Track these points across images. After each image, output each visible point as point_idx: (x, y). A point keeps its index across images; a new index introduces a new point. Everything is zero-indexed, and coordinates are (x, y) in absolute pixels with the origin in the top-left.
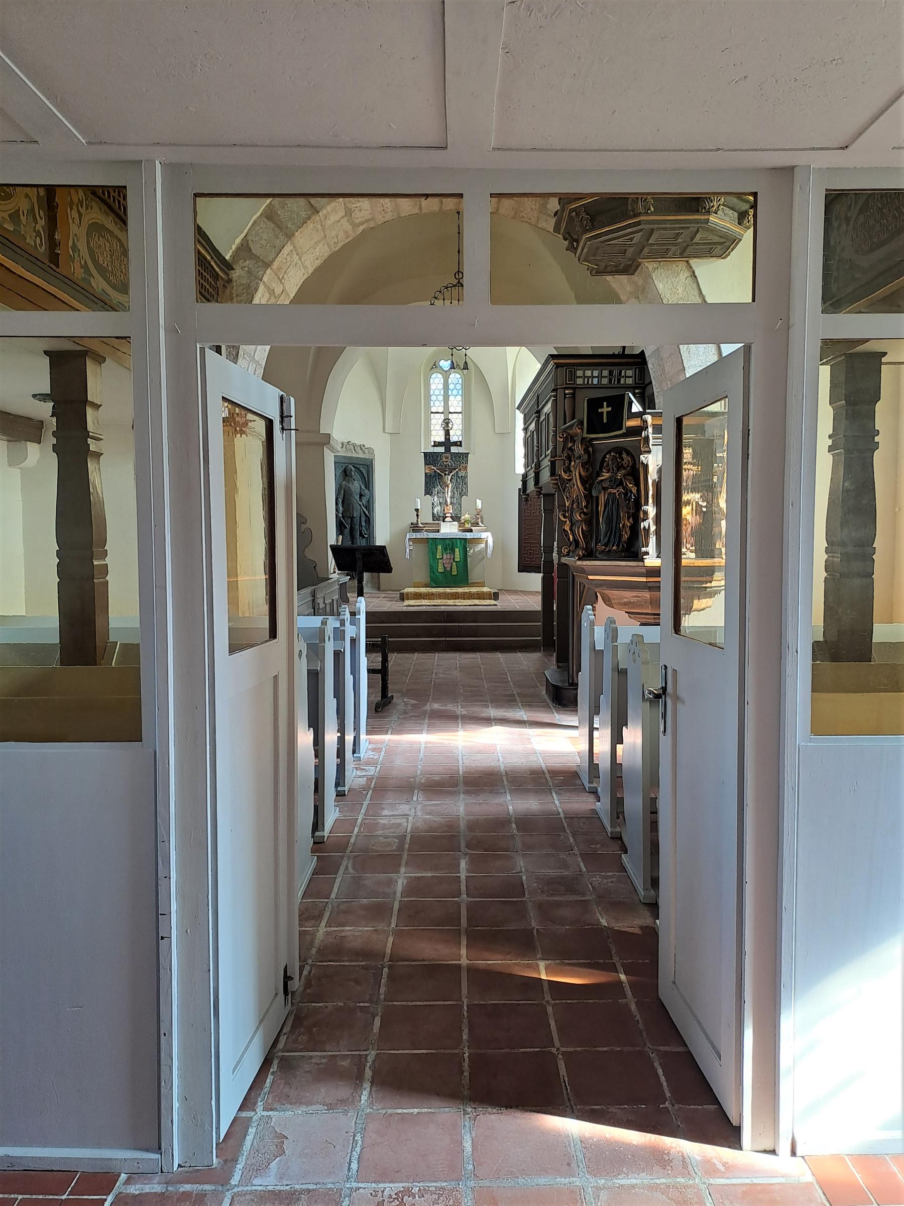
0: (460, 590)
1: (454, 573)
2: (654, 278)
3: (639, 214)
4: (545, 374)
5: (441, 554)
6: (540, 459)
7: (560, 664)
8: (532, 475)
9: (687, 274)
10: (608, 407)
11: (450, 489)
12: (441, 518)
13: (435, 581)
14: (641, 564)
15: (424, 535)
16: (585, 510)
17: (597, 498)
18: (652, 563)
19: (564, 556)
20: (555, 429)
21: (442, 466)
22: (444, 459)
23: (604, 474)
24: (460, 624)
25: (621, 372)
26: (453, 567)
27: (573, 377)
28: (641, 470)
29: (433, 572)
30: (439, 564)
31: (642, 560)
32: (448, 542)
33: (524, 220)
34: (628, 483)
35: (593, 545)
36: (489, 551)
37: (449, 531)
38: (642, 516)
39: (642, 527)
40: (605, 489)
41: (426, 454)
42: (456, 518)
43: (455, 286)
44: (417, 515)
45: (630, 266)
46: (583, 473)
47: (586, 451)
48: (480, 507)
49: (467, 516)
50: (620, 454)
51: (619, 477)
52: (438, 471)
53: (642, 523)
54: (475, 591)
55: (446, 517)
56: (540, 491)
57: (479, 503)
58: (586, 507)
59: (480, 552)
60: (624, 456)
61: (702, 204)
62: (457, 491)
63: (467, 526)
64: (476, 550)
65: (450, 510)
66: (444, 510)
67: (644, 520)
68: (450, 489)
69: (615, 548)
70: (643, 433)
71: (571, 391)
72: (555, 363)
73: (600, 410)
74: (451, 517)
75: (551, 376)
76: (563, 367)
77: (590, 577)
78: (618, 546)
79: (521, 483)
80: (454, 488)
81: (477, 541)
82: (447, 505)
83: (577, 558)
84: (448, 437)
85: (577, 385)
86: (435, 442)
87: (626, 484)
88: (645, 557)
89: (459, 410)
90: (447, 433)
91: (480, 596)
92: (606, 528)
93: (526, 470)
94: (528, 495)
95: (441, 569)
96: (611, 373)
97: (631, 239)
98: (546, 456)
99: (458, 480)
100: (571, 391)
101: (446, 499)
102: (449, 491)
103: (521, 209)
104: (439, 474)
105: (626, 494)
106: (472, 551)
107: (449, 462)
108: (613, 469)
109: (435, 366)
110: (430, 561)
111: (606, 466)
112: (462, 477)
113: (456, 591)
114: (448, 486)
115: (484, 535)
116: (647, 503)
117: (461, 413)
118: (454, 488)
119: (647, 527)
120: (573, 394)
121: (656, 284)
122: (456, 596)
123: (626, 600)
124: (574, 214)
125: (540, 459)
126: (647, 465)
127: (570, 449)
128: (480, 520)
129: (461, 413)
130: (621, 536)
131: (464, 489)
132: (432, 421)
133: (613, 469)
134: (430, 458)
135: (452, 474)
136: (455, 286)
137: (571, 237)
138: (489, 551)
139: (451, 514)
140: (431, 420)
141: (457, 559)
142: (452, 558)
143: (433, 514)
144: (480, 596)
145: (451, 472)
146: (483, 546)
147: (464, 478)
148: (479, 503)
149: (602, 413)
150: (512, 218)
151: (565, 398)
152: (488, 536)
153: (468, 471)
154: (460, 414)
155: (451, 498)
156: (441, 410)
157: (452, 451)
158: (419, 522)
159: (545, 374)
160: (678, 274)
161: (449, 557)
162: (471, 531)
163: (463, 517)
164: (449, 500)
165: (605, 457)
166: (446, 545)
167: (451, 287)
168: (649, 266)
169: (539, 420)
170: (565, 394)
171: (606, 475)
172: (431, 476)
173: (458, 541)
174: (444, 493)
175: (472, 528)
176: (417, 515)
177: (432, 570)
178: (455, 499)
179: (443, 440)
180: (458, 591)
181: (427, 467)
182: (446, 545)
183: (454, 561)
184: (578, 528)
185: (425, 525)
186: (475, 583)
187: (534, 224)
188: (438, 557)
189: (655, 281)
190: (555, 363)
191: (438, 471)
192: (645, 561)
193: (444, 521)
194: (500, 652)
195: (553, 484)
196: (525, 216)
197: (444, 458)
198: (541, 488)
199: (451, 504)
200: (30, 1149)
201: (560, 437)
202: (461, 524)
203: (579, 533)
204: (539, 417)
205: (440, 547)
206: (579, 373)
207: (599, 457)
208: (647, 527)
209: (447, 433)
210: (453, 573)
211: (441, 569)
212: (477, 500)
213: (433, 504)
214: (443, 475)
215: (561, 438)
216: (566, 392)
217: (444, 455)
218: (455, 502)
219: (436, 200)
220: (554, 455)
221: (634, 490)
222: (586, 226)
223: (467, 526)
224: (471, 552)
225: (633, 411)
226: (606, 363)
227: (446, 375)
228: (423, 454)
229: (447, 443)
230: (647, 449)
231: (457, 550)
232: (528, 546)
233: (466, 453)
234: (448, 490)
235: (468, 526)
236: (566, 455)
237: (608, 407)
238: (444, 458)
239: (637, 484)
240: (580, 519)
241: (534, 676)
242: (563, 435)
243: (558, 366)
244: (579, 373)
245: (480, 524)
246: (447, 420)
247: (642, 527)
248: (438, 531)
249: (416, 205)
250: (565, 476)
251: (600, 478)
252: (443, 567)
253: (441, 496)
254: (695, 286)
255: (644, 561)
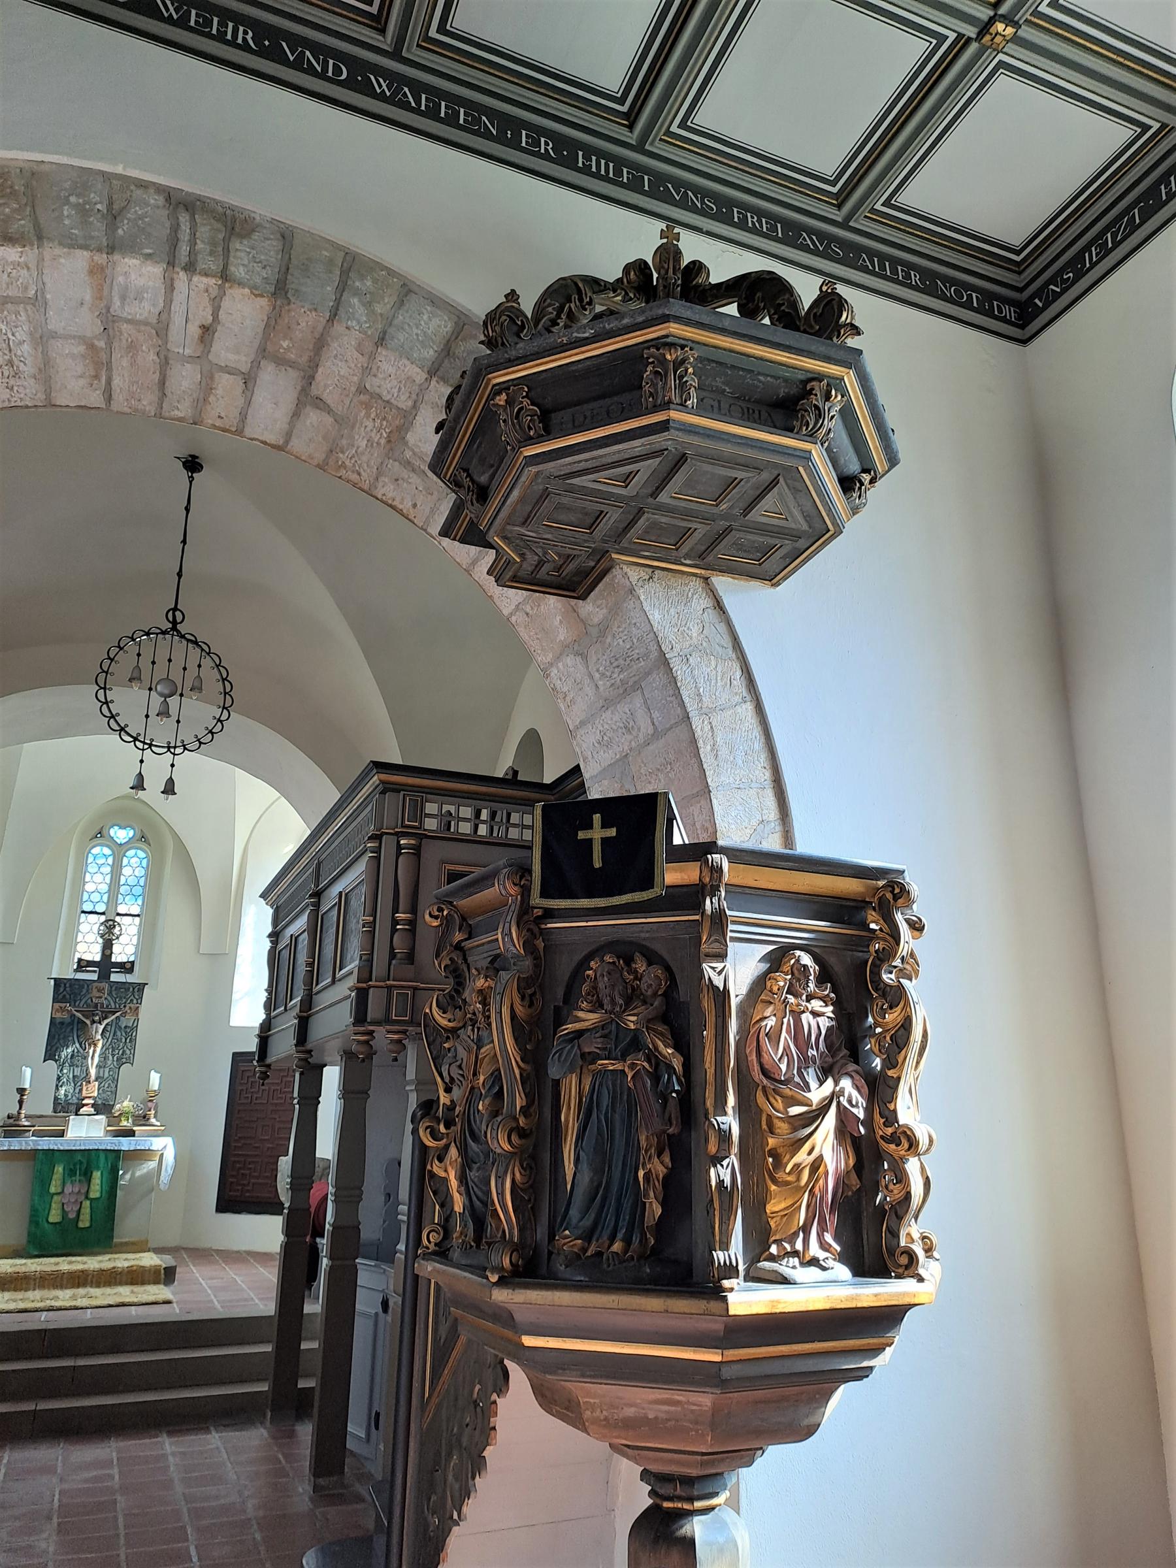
0: (92, 1263)
1: (85, 1223)
2: (642, 598)
3: (666, 405)
4: (295, 871)
5: (59, 1183)
6: (273, 1014)
7: (321, 1481)
8: (288, 1023)
9: (706, 602)
10: (604, 826)
11: (98, 1050)
12: (73, 1108)
13: (38, 1246)
14: (714, 1306)
15: (29, 1142)
16: (522, 1121)
17: (557, 1083)
18: (750, 1304)
19: (427, 1256)
20: (371, 918)
21: (88, 1006)
22: (95, 993)
23: (581, 1014)
24: (81, 1362)
25: (509, 815)
26: (83, 1211)
27: (419, 814)
28: (707, 1003)
29: (37, 1224)
30: (53, 1205)
31: (718, 1294)
32: (79, 1157)
33: (342, 472)
34: (660, 1044)
35: (542, 1232)
36: (165, 1177)
37: (84, 1135)
38: (712, 1148)
39: (713, 1183)
40: (589, 1058)
41: (58, 982)
42: (102, 1108)
43: (164, 633)
44: (21, 1102)
45: (587, 573)
46: (520, 1010)
47: (528, 945)
48: (156, 1088)
49: (126, 1103)
50: (629, 961)
51: (632, 1026)
52: (79, 1015)
53: (712, 1171)
54: (126, 1264)
55: (84, 1105)
56: (306, 1060)
57: (155, 1079)
58: (525, 1111)
59: (148, 1176)
60: (640, 965)
61: (803, 416)
62: (113, 1055)
63: (124, 1123)
64: (138, 1174)
65: (92, 1090)
66: (81, 1090)
67: (717, 1160)
68: (98, 1050)
69: (617, 1247)
70: (708, 901)
71: (413, 842)
72: (382, 782)
73: (581, 835)
74: (93, 1105)
75: (369, 808)
76: (399, 791)
77: (528, 1341)
78: (628, 1241)
79: (256, 1040)
80: (107, 1049)
81: (141, 1155)
82: (89, 1082)
83: (494, 1278)
84: (108, 952)
85: (425, 830)
86: (80, 960)
87: (656, 1048)
88: (726, 1283)
89: (136, 910)
90: (108, 946)
91: (136, 1277)
92: (592, 1181)
93: (268, 1015)
94: (269, 1066)
95: (55, 1216)
96: (493, 815)
97: (627, 479)
98: (334, 982)
99: (119, 1033)
100: (413, 842)
101: (87, 1069)
102: (97, 1055)
103: (344, 442)
104: (80, 1021)
105: (656, 1078)
106: (128, 1177)
107: (105, 1000)
108: (613, 1002)
109: (100, 835)
110: (32, 1200)
111: (588, 994)
112: (126, 1027)
113: (80, 1267)
114: (95, 1045)
115: (157, 1143)
116: (721, 1109)
117: (138, 916)
118: (107, 1049)
119: (727, 1181)
120: (417, 851)
121: (647, 609)
122: (79, 1280)
123: (630, 1412)
124: (501, 399)
125: (273, 1014)
126: (725, 993)
127: (458, 947)
128: (153, 1112)
129: (138, 916)
130: (639, 1207)
131: (128, 1052)
132: (81, 928)
133: (613, 1002)
134: (64, 990)
135: (106, 1022)
136: (164, 633)
137: (472, 480)
138: (165, 1177)
139: (94, 1098)
140: (79, 924)
141: (92, 1195)
142: (84, 1191)
143: (56, 1099)
144: (136, 1277)
145: (106, 1018)
146: (152, 1165)
147: (130, 1033)
148: (155, 1079)
149: (589, 842)
150: (318, 466)
151: (399, 854)
152: (165, 1146)
153: (140, 1016)
154: (137, 919)
155: (99, 1067)
156: (101, 908)
157: (112, 980)
158: (23, 1116)
159: (295, 871)
160: (688, 601)
161: (77, 1190)
162: (130, 1133)
163: (118, 1107)
164: (93, 1072)
165: (584, 964)
166: (75, 1165)
167: (157, 634)
168: (630, 573)
169: (317, 911)
170: (399, 847)
171: (588, 1018)
172: (62, 1023)
173: (102, 1156)
174: (85, 1058)
175: (135, 1128)
176: (21, 1102)
177: (35, 1217)
178: (107, 1070)
179: (98, 958)
180: (85, 1267)
181: (57, 1005)
182: (75, 1165)
183: (87, 1198)
184: (501, 1179)
185: (35, 1121)
186: (126, 1244)
187: (366, 487)
188: (53, 1190)
189: (645, 604)
190: (382, 782)
191: (79, 1015)
192: (731, 1297)
193: (77, 1115)
194: (170, 1433)
195: (359, 1042)
196: (347, 463)
197: (95, 991)
198: (309, 1052)
199: (96, 1080)
200: (1055, 12)
201: (431, 915)
202: (113, 1119)
203: (501, 1194)
204: (317, 905)
205: (59, 1169)
206: (431, 808)
207: (564, 967)
208: (727, 1181)
209: (108, 946)
210: (81, 1225)
211: (55, 1216)
212: (153, 1072)
213: (59, 1079)
214: (88, 1022)
215: (436, 917)
216: (402, 842)
217: (95, 984)
218: (106, 1075)
219: (130, 918)
220: (366, 975)
221: (677, 1063)
222: (530, 428)
223: (124, 1123)
224: (125, 1179)
225: (677, 840)
226: (485, 794)
227: (119, 851)
228: (52, 981)
229: (106, 965)
230: (715, 948)
231: (97, 1175)
232: (239, 1162)
233: (139, 984)
234: (94, 1051)
235: (126, 1123)
236: (447, 961)
237: (604, 826)
238: (95, 991)
239: (682, 1045)
240: (507, 1147)
241: (258, 1536)
242: (440, 910)
243: (386, 788)
244: (431, 808)
245: (153, 1120)
246: (111, 923)
247: (713, 1183)
248: (62, 1134)
249: (97, 377)
250: (442, 1020)
251: (571, 1027)
252: (59, 1212)
253: (79, 1064)
254: (722, 628)
255: (725, 1299)
